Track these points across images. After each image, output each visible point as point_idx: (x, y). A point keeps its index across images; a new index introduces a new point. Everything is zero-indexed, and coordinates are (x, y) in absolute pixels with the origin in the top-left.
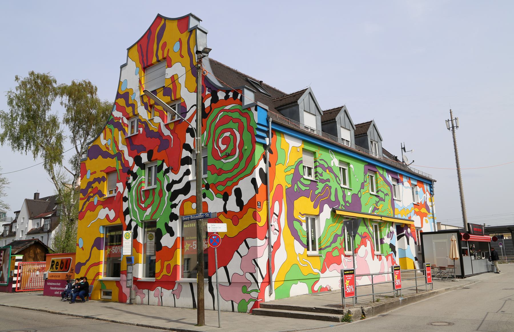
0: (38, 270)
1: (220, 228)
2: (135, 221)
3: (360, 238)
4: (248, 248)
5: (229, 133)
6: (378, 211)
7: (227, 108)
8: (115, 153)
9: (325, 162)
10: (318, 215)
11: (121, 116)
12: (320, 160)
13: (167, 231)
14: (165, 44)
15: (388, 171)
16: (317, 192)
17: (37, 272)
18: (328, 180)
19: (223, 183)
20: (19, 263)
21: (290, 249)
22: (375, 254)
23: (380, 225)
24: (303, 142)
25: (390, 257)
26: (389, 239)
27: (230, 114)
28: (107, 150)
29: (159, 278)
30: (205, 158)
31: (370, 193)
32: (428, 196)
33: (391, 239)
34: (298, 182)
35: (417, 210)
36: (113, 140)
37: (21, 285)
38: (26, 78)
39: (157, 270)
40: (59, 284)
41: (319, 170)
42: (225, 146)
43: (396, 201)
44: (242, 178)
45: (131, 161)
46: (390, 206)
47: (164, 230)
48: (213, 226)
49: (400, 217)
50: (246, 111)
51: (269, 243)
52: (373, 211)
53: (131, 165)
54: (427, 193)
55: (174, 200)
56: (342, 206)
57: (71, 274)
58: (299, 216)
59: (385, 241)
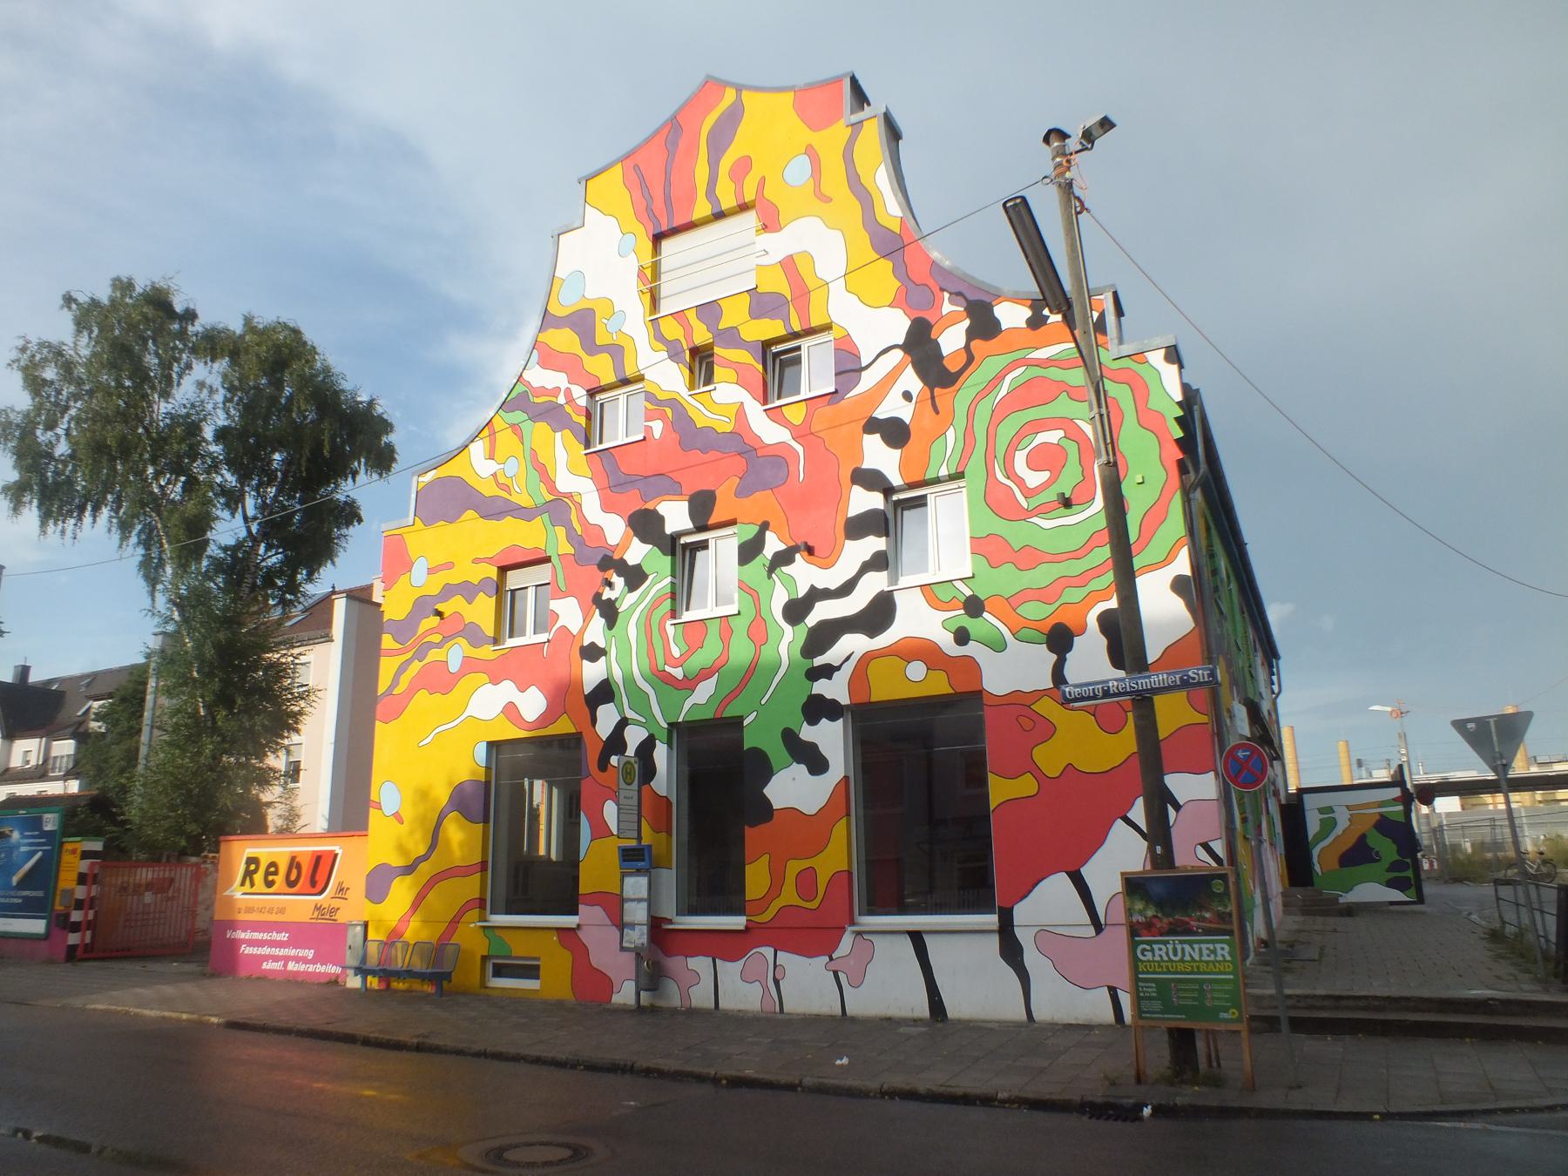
0: (149, 886)
5: (1061, 433)
13: (792, 757)
17: (147, 894)
27: (1054, 373)
28: (504, 495)
30: (540, 588)
36: (528, 459)
37: (93, 937)
38: (33, 347)
40: (284, 936)
45: (614, 528)
55: (822, 652)
57: (336, 903)
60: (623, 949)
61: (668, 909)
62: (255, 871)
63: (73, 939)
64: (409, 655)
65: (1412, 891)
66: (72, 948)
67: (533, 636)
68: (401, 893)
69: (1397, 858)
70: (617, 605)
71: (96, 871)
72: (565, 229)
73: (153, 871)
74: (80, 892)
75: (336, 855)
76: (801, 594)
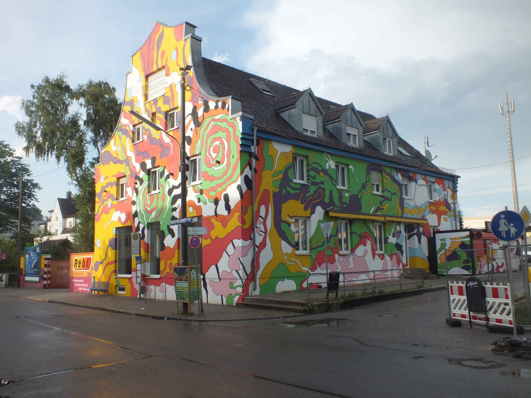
1: (200, 231)
2: (143, 223)
3: (358, 238)
4: (235, 248)
6: (383, 211)
7: (217, 117)
8: (124, 159)
9: (319, 164)
10: (309, 217)
11: (128, 123)
12: (313, 163)
14: (163, 53)
15: (398, 170)
16: (308, 195)
17: (65, 270)
18: (322, 183)
19: (214, 189)
20: (48, 261)
21: (276, 248)
22: (376, 254)
23: (384, 225)
24: (293, 147)
25: (395, 257)
26: (395, 239)
27: (219, 123)
28: (117, 156)
29: (163, 275)
31: (373, 194)
32: (450, 193)
33: (397, 239)
34: (287, 187)
35: (433, 208)
37: (51, 282)
39: (162, 267)
40: (82, 281)
41: (312, 173)
42: (216, 154)
43: (406, 200)
44: (229, 185)
45: (138, 167)
46: (398, 206)
47: (166, 232)
48: (193, 230)
49: (410, 216)
50: (232, 120)
51: (254, 244)
52: (376, 211)
53: (138, 170)
54: (449, 190)
56: (338, 208)
57: (91, 272)
58: (287, 218)
59: (390, 241)
60: (137, 283)
61: (148, 273)
62: (77, 263)
63: (45, 282)
64: (101, 203)
65: (471, 271)
66: (45, 285)
67: (198, 181)
68: (101, 268)
69: (467, 258)
70: (138, 189)
71: (49, 264)
72: (128, 73)
73: (65, 263)
74: (46, 270)
75: (91, 259)
76: (171, 187)
